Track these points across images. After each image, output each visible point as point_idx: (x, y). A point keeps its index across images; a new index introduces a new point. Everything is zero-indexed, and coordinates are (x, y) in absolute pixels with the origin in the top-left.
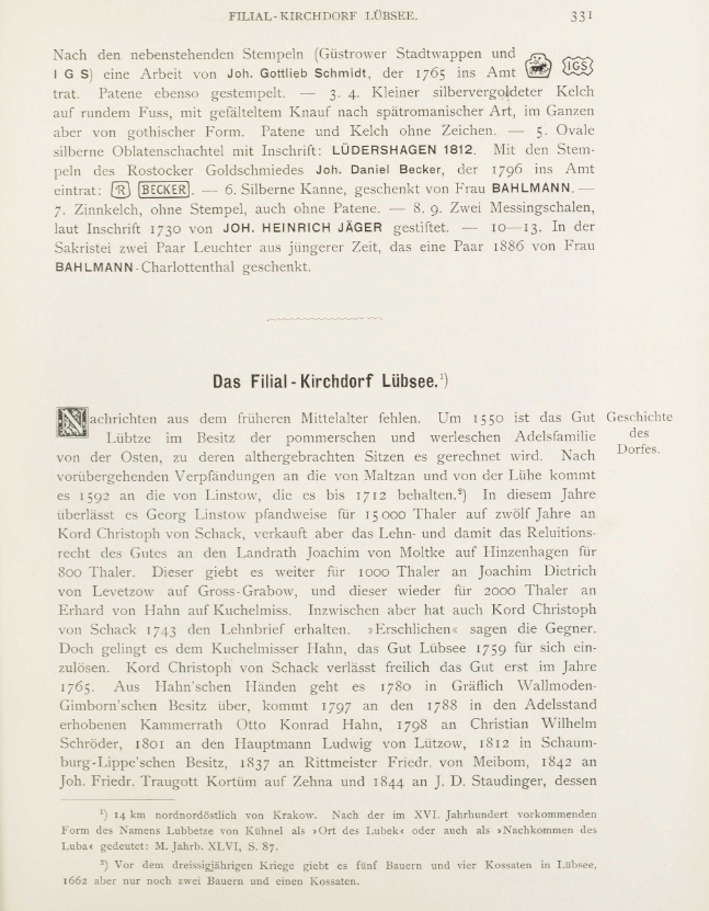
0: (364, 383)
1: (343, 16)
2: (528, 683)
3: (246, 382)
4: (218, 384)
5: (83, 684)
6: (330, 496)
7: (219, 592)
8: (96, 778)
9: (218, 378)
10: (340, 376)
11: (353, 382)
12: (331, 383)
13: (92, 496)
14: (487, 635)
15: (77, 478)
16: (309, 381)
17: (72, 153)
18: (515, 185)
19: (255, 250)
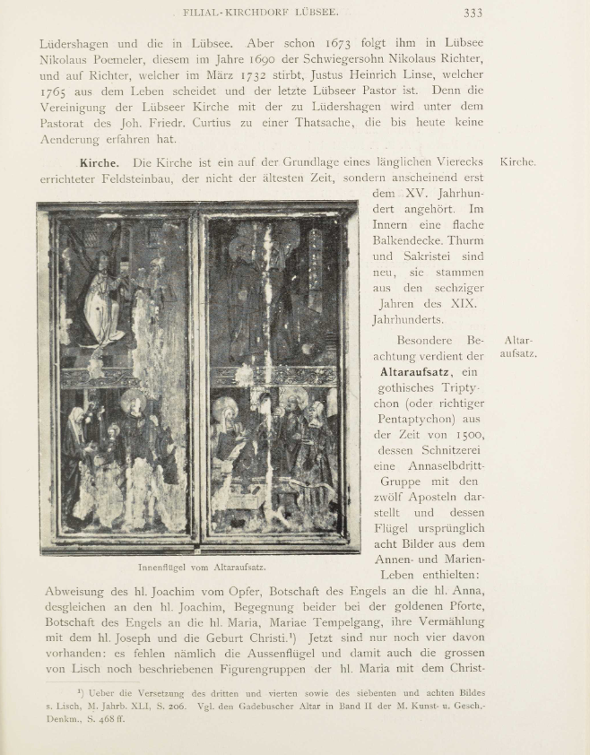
1: (277, 12)
5: (60, 90)
6: (394, 123)
7: (459, 654)
8: (106, 176)
13: (466, 435)
14: (396, 166)
15: (445, 529)
17: (455, 467)
19: (399, 92)
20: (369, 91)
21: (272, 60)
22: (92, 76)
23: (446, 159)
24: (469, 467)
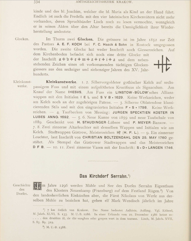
0: (106, 177)
2: (149, 195)
3: (88, 176)
4: (81, 177)
9: (81, 175)
10: (100, 175)
11: (104, 176)
12: (97, 176)
13: (125, 118)
16: (92, 176)
18: (127, 137)
20: (44, 44)
21: (165, 138)
22: (131, 17)
23: (95, 147)
24: (120, 55)
